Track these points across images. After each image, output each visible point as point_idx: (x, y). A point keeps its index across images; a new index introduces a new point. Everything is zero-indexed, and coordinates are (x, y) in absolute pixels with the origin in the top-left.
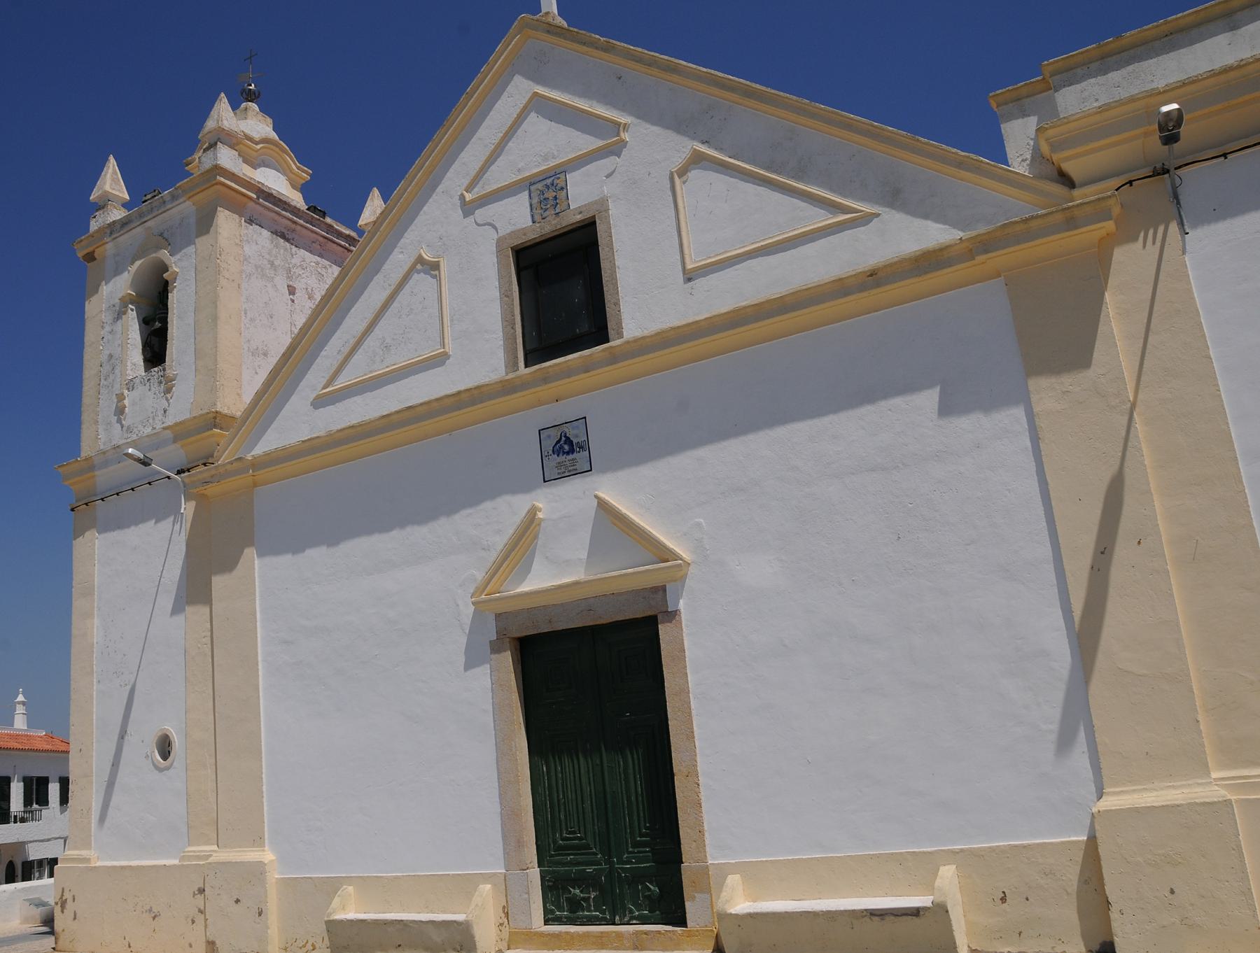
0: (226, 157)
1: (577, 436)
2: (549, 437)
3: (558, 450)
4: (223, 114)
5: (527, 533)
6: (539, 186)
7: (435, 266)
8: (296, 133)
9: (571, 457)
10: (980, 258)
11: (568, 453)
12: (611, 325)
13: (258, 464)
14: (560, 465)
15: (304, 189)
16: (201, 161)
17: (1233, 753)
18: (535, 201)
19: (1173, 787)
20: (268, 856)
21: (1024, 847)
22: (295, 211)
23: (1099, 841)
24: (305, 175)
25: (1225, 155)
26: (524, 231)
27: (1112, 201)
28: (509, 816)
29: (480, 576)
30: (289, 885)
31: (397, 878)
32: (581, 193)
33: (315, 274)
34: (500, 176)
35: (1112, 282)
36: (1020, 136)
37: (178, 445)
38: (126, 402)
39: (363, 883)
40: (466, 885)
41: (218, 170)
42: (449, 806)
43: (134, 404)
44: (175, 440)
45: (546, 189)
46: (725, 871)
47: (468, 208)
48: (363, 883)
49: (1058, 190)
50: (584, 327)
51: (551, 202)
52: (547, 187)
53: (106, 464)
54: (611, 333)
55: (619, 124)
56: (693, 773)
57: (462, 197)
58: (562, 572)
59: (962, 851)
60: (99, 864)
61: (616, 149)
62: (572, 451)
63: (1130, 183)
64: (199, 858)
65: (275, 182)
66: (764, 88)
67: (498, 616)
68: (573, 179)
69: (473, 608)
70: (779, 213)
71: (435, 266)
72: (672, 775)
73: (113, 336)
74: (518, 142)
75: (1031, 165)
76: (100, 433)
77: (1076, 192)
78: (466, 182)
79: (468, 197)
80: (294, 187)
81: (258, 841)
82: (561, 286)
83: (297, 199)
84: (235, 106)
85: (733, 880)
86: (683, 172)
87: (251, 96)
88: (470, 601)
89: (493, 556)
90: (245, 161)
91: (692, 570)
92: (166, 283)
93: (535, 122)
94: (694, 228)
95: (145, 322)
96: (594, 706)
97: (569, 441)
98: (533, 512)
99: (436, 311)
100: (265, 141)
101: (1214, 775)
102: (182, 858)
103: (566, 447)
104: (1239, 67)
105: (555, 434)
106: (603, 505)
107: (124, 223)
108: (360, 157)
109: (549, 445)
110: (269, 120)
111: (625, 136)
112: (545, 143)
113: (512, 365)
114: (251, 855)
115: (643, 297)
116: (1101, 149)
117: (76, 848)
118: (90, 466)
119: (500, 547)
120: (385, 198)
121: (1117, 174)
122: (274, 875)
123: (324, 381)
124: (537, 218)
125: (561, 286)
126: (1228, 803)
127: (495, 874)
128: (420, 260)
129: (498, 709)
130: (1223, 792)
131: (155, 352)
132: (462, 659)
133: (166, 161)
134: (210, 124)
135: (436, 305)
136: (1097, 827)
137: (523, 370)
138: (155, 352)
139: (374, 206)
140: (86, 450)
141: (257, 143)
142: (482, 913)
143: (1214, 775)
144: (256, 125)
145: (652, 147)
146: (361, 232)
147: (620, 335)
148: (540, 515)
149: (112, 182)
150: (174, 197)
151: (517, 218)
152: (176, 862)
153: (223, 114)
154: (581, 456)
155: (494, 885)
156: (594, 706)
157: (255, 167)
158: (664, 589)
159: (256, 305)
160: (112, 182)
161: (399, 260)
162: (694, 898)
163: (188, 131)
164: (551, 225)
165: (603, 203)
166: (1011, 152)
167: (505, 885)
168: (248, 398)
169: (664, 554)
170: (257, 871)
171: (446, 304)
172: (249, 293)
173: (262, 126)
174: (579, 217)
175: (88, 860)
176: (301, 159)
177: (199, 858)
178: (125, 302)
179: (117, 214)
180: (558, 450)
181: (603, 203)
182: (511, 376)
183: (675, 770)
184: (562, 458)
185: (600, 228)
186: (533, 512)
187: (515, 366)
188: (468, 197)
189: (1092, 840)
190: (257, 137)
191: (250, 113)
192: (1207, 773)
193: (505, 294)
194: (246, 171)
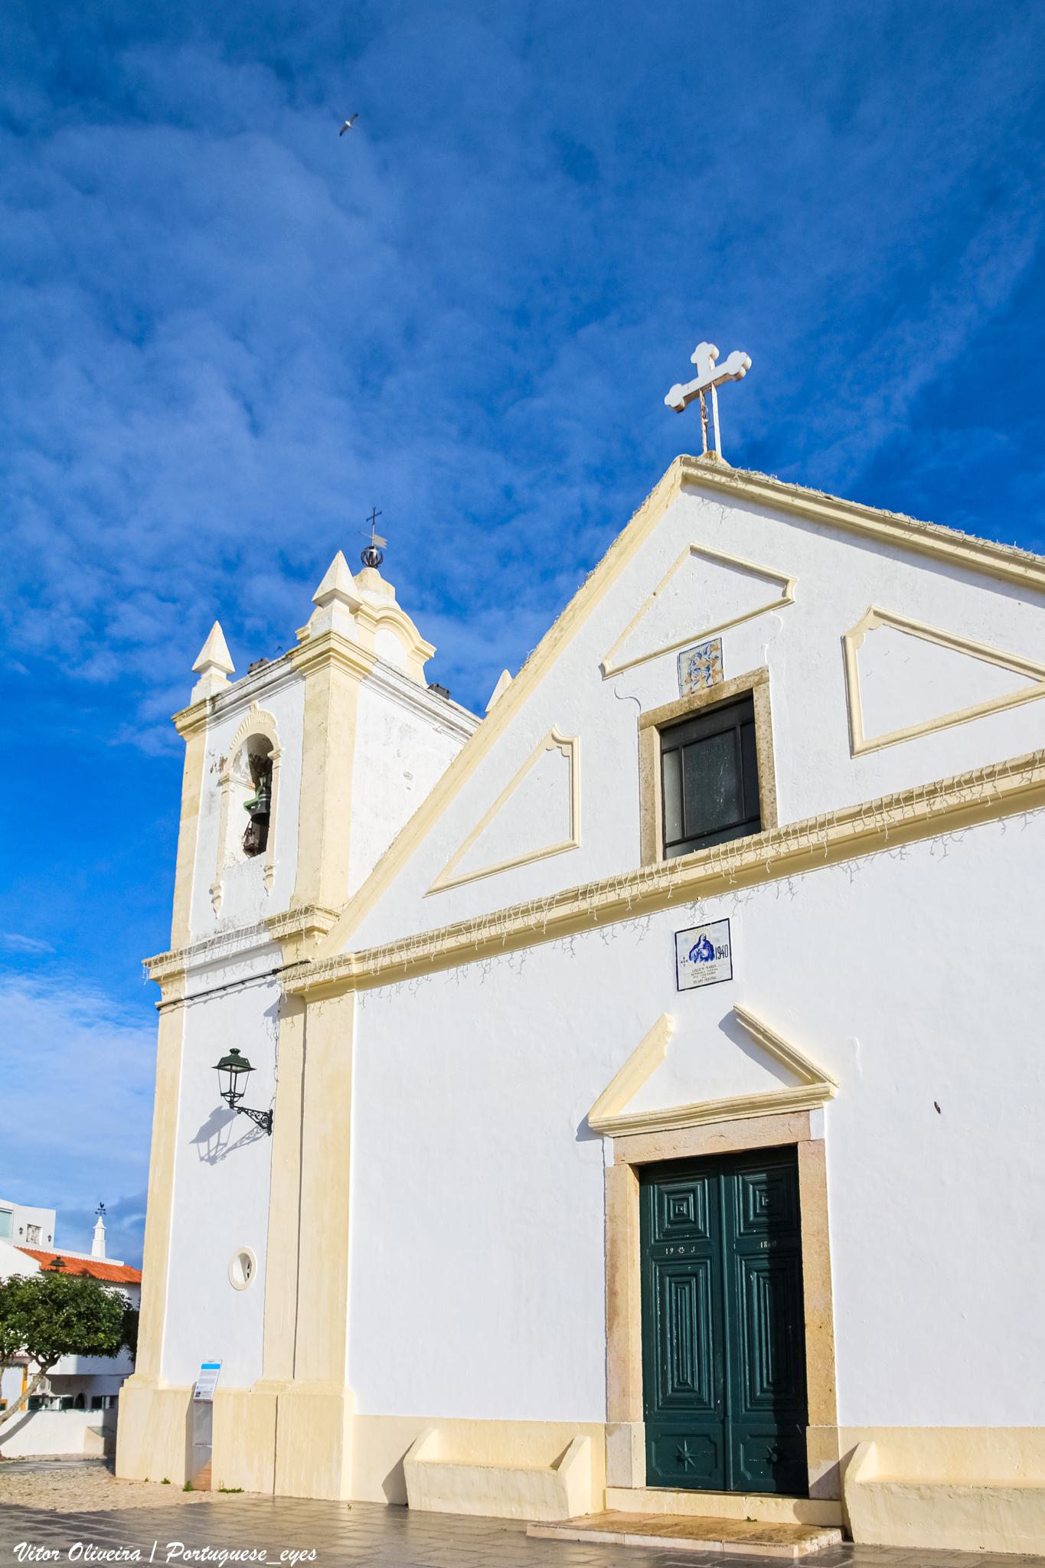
1: (718, 940)
2: (686, 940)
3: (695, 956)
9: (710, 963)
11: (706, 959)
12: (766, 812)
14: (696, 972)
16: (313, 627)
42: (535, 1385)
45: (704, 656)
52: (700, 655)
54: (766, 821)
56: (826, 1323)
58: (694, 1090)
62: (711, 956)
74: (693, 575)
76: (193, 917)
82: (713, 762)
84: (355, 571)
87: (374, 563)
96: (726, 1272)
97: (708, 945)
103: (705, 953)
105: (693, 938)
108: (489, 594)
109: (685, 949)
110: (393, 589)
112: (701, 602)
115: (800, 777)
120: (513, 676)
125: (713, 762)
131: (257, 842)
138: (257, 842)
147: (774, 824)
151: (667, 692)
154: (720, 964)
156: (726, 1272)
164: (701, 694)
180: (695, 956)
184: (700, 964)
187: (652, 859)
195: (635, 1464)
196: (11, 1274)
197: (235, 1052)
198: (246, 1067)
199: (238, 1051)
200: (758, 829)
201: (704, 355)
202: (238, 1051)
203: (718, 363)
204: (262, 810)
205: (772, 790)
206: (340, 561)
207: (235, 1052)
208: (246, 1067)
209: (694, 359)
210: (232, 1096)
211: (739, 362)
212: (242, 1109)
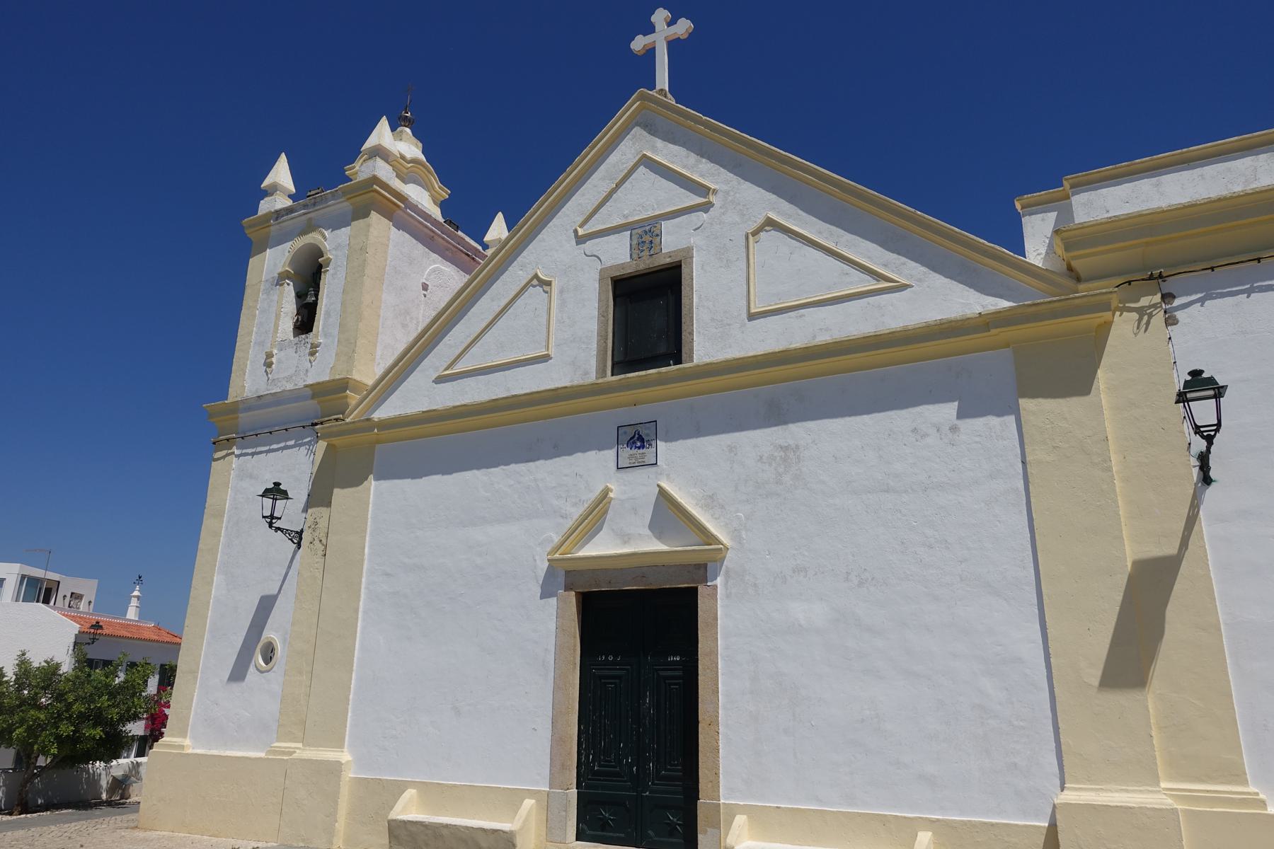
0: (383, 170)
4: (382, 135)
5: (596, 515)
6: (639, 231)
7: (549, 284)
8: (442, 159)
9: (641, 451)
10: (994, 331)
13: (387, 425)
15: (444, 206)
16: (361, 170)
17: (1185, 767)
18: (635, 242)
19: (1127, 791)
20: (345, 756)
21: (993, 825)
22: (435, 222)
23: (1059, 829)
24: (445, 194)
25: (1212, 269)
26: (622, 266)
27: (1114, 296)
28: (557, 741)
29: (556, 539)
30: (359, 782)
31: (455, 786)
32: (672, 240)
33: (447, 278)
34: (611, 216)
35: (1105, 361)
36: (1038, 236)
37: (315, 402)
38: (274, 360)
39: (423, 787)
40: (513, 799)
41: (375, 180)
42: (505, 743)
43: (279, 361)
44: (313, 397)
45: (645, 233)
46: (733, 811)
47: (580, 240)
48: (423, 787)
49: (1070, 283)
50: (662, 349)
51: (647, 245)
53: (249, 409)
54: (684, 356)
55: (709, 189)
56: (714, 722)
57: (576, 231)
58: (627, 541)
59: (938, 820)
60: (190, 751)
61: (706, 207)
62: (643, 447)
63: (1129, 282)
64: (284, 753)
65: (416, 194)
66: (643, 373)
67: (567, 573)
68: (666, 226)
69: (547, 564)
70: (830, 277)
71: (549, 284)
72: (698, 722)
73: (267, 307)
74: (642, 183)
75: (1045, 259)
76: (248, 380)
77: (1081, 286)
78: (581, 219)
79: (581, 232)
80: (435, 203)
81: (340, 745)
82: (648, 310)
83: (436, 213)
84: (393, 129)
85: (740, 820)
86: (755, 233)
88: (546, 558)
89: (569, 524)
90: (398, 176)
91: (729, 555)
92: (320, 266)
93: (642, 169)
94: (773, 263)
95: (300, 296)
96: (639, 659)
98: (606, 492)
99: (544, 321)
100: (415, 161)
101: (1163, 785)
102: (268, 752)
104: (1231, 198)
105: (631, 432)
106: (663, 493)
107: (289, 210)
110: (420, 145)
111: (712, 198)
112: (647, 197)
113: (601, 372)
114: (329, 755)
115: (717, 329)
116: (1108, 251)
117: (172, 736)
118: (235, 408)
119: (575, 517)
121: (1119, 274)
122: (350, 774)
123: (445, 365)
124: (635, 256)
125: (648, 310)
126: (1174, 811)
127: (539, 791)
128: (536, 276)
129: (559, 649)
130: (1170, 801)
131: (305, 324)
132: (539, 591)
133: (327, 167)
134: (371, 142)
135: (546, 317)
136: (1058, 817)
137: (610, 378)
138: (305, 324)
139: (498, 229)
140: (234, 395)
141: (409, 162)
142: (524, 820)
143: (1163, 785)
144: (408, 147)
145: (742, 199)
146: (486, 247)
148: (611, 495)
149: (281, 174)
150: (334, 196)
151: (618, 254)
152: (262, 755)
153: (382, 135)
155: (538, 801)
156: (639, 659)
157: (405, 181)
158: (705, 566)
159: (382, 287)
160: (281, 174)
161: (516, 275)
162: (706, 832)
163: (352, 146)
165: (688, 251)
166: (1028, 246)
167: (547, 803)
168: (379, 371)
169: (709, 538)
170: (335, 769)
171: (551, 312)
172: (390, 282)
173: (414, 148)
174: (668, 260)
175: (182, 747)
176: (443, 181)
177: (284, 753)
178: (281, 279)
179: (282, 202)
181: (688, 251)
182: (600, 381)
183: (700, 718)
184: (634, 451)
185: (685, 270)
186: (606, 492)
188: (581, 232)
189: (1053, 828)
190: (408, 156)
191: (404, 136)
192: (1158, 785)
193: (602, 315)
194: (397, 184)
195: (569, 823)
196: (47, 656)
197: (1196, 374)
198: (285, 495)
199: (1201, 372)
200: (678, 361)
201: (660, 16)
202: (1201, 372)
203: (669, 24)
204: (311, 299)
205: (691, 333)
206: (384, 124)
207: (277, 484)
208: (285, 495)
209: (653, 19)
210: (271, 519)
211: (684, 27)
212: (278, 529)
